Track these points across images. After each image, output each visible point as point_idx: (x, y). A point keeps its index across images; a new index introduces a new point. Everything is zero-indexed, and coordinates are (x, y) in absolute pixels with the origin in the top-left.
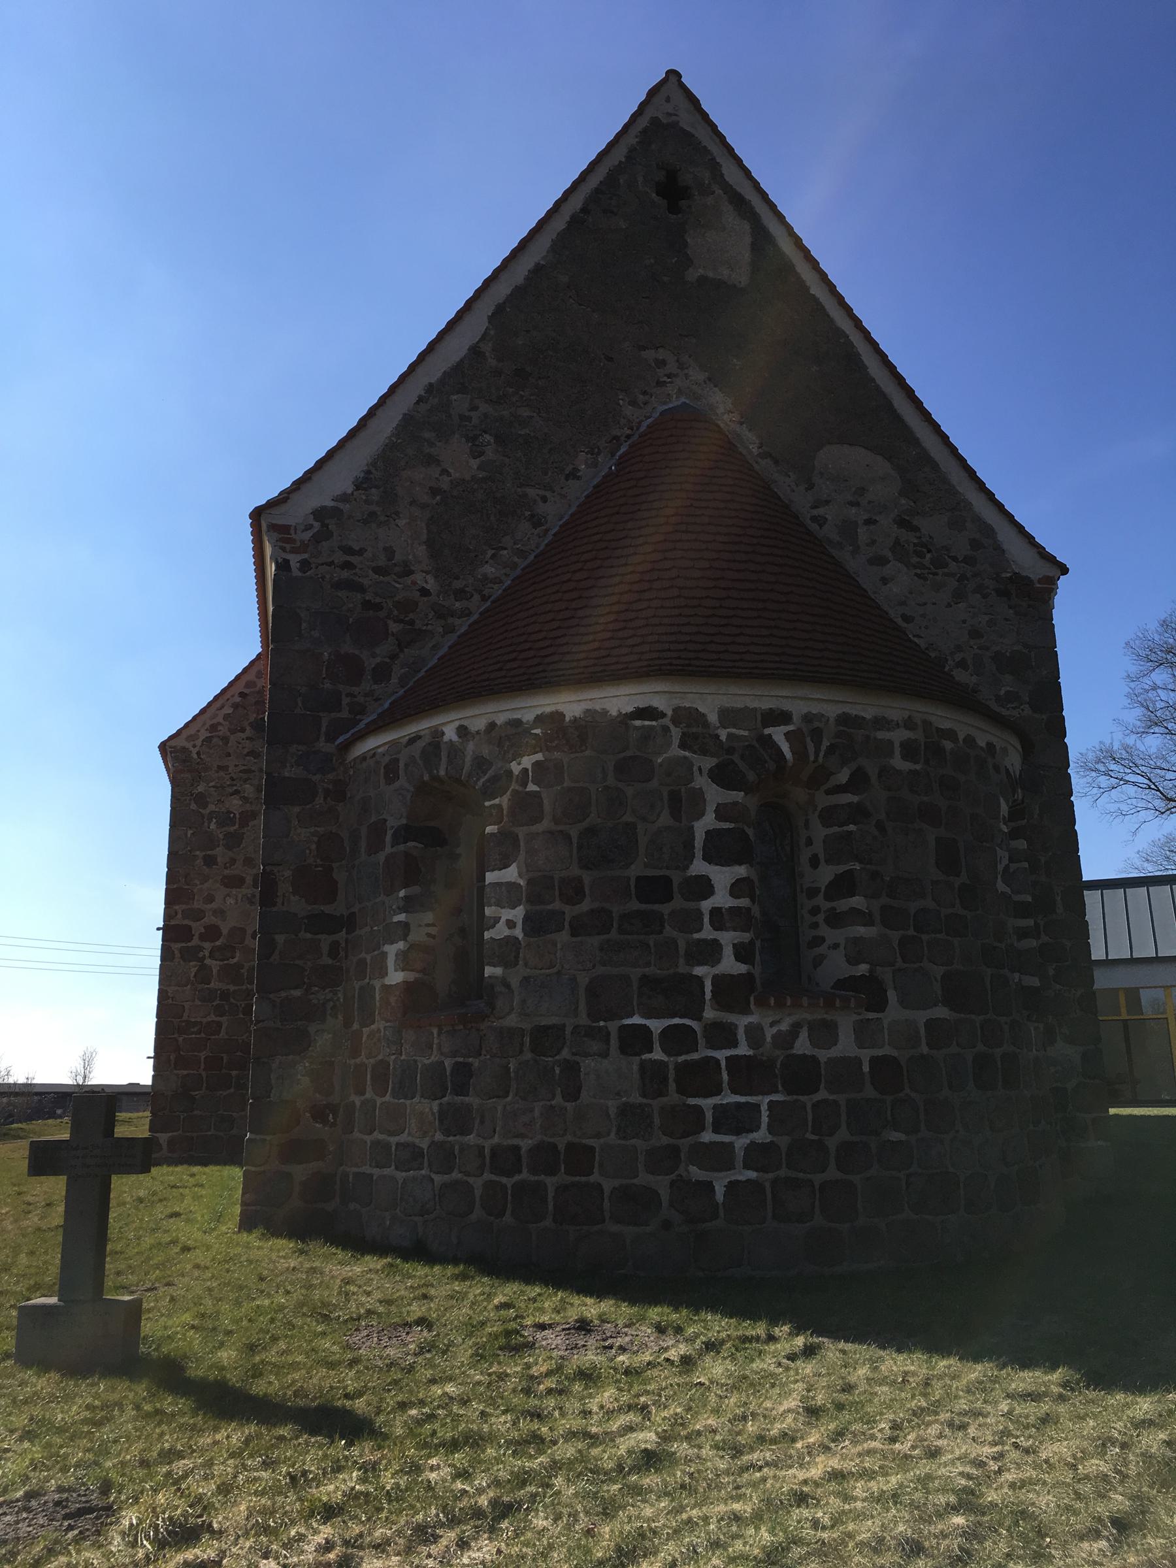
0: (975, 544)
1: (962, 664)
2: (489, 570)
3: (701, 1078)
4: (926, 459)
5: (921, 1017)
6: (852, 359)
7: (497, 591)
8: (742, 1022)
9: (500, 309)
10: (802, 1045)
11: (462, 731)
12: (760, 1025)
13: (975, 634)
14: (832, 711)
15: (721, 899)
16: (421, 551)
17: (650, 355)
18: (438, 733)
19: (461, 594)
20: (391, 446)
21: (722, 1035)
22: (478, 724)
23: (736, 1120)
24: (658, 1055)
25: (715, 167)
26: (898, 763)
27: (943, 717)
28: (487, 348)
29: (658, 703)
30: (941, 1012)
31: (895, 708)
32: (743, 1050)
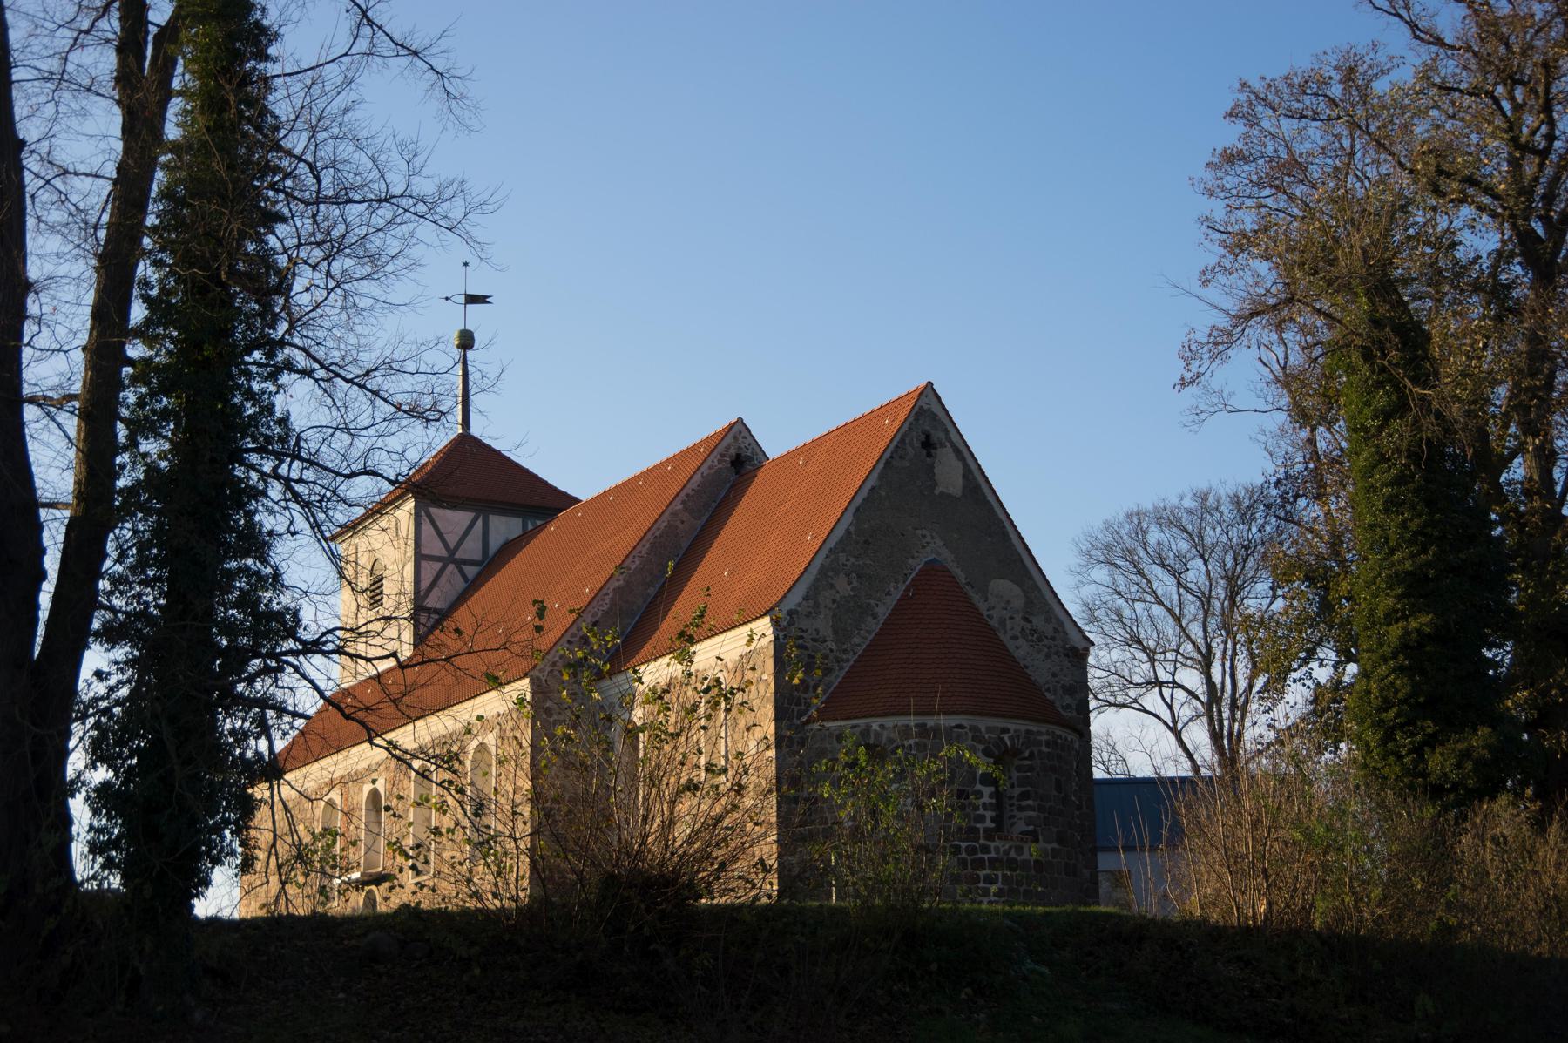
0: (1056, 630)
1: (1048, 690)
2: (856, 640)
3: (979, 864)
4: (1036, 587)
5: (1049, 847)
6: (1005, 535)
7: (860, 651)
8: (992, 845)
9: (858, 510)
10: (1013, 854)
11: (882, 726)
12: (997, 846)
13: (1054, 675)
14: (1023, 728)
15: (986, 799)
16: (830, 631)
17: (919, 532)
18: (869, 726)
19: (845, 651)
20: (817, 580)
21: (986, 849)
22: (891, 725)
23: (990, 880)
24: (964, 855)
25: (947, 432)
26: (1044, 749)
27: (1058, 731)
28: (852, 529)
29: (965, 723)
30: (1055, 845)
31: (1043, 728)
32: (993, 855)
